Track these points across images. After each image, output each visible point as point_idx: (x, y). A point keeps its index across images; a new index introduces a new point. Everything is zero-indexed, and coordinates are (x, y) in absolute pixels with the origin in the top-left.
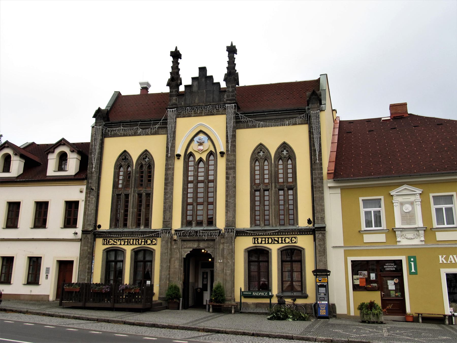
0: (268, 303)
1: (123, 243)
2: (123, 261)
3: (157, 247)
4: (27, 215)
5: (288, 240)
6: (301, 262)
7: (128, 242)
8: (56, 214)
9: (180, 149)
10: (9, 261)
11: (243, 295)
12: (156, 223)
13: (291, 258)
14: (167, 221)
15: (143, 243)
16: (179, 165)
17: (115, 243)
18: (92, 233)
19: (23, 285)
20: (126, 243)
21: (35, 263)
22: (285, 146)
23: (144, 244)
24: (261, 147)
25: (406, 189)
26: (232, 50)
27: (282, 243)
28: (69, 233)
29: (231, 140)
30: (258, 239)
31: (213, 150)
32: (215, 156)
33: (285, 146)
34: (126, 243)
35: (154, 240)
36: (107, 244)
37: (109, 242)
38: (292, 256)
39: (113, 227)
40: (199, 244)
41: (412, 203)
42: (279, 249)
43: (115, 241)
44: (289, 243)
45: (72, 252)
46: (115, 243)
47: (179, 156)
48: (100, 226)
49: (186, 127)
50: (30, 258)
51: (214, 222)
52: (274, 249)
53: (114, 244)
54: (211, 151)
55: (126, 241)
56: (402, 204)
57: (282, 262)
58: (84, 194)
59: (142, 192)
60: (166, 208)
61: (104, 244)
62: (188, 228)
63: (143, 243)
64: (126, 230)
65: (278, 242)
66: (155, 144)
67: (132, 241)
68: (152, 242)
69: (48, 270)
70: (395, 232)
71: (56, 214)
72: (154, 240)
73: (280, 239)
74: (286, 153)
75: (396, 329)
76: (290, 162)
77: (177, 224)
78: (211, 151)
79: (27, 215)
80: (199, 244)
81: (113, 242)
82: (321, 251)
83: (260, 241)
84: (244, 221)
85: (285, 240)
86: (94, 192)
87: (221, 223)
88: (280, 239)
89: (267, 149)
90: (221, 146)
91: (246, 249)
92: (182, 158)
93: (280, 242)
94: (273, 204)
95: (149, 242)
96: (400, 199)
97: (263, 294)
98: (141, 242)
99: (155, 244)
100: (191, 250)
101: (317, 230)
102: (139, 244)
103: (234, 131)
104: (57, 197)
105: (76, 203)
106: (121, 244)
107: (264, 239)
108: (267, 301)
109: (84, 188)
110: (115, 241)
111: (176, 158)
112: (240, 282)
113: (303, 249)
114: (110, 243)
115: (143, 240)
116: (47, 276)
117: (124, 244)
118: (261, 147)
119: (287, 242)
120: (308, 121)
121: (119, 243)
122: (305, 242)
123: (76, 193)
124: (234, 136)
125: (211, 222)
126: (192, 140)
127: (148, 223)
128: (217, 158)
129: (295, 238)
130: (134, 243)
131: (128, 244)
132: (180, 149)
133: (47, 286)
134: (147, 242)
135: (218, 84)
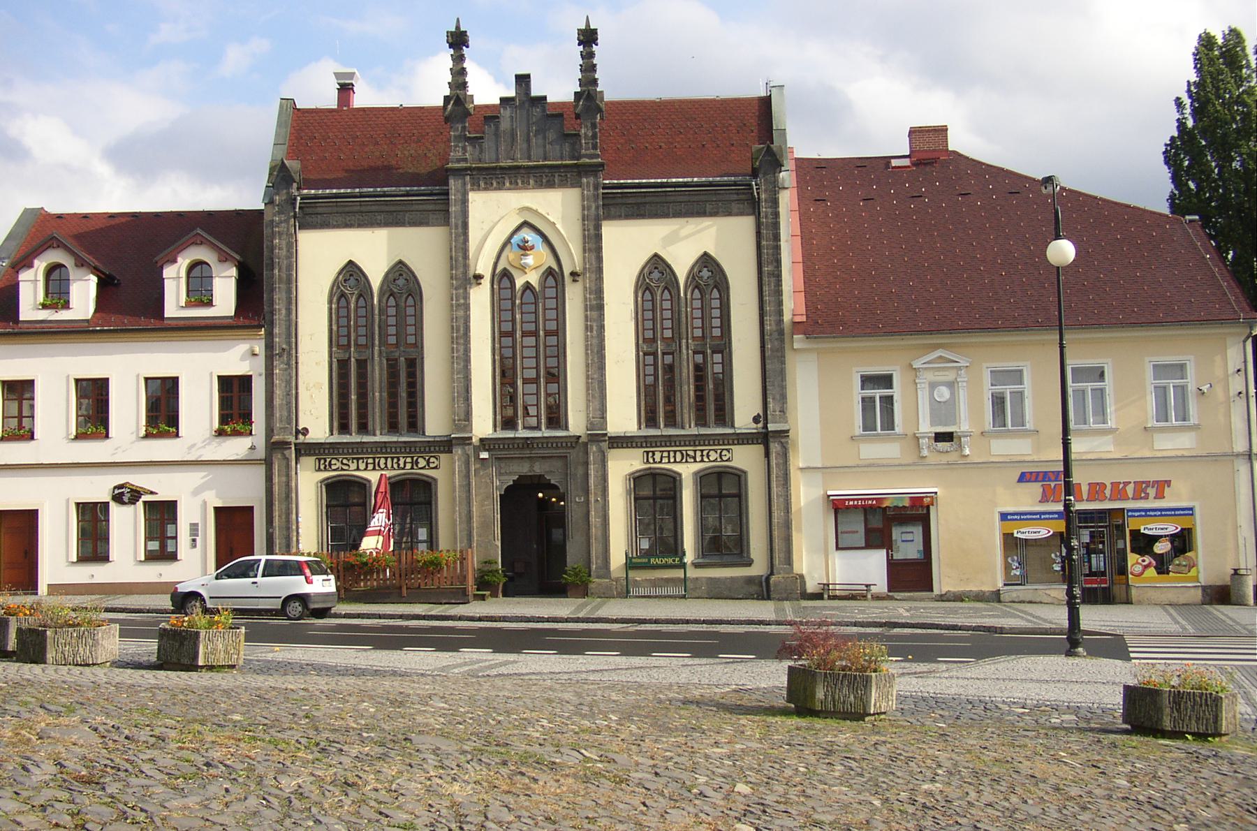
0: (679, 579)
1: (362, 466)
3: (443, 474)
4: (127, 408)
5: (713, 456)
6: (740, 496)
8: (198, 407)
9: (483, 264)
10: (27, 521)
11: (630, 565)
12: (435, 423)
13: (720, 490)
15: (408, 466)
16: (480, 299)
18: (283, 449)
20: (370, 467)
22: (706, 260)
24: (657, 264)
25: (941, 357)
26: (588, 38)
27: (702, 461)
28: (237, 447)
29: (593, 244)
30: (653, 453)
31: (555, 267)
32: (560, 279)
33: (706, 260)
34: (370, 467)
35: (432, 460)
37: (330, 464)
38: (722, 489)
39: (335, 432)
40: (532, 466)
41: (951, 385)
42: (696, 474)
44: (715, 460)
47: (478, 277)
48: (305, 432)
49: (492, 214)
51: (419, 424)
52: (687, 471)
54: (550, 268)
55: (370, 461)
56: (933, 386)
57: (703, 498)
58: (261, 360)
59: (397, 354)
60: (466, 391)
61: (319, 470)
62: (510, 434)
63: (408, 466)
64: (366, 439)
65: (694, 458)
66: (419, 247)
67: (383, 461)
68: (428, 462)
69: (194, 528)
70: (918, 438)
71: (198, 407)
72: (432, 460)
73: (698, 453)
74: (709, 273)
75: (916, 609)
76: (715, 294)
77: (483, 424)
78: (550, 268)
79: (127, 408)
80: (532, 466)
81: (339, 465)
82: (777, 478)
83: (657, 458)
84: (623, 415)
85: (708, 456)
86: (281, 354)
87: (576, 423)
88: (698, 453)
89: (669, 266)
90: (573, 257)
91: (630, 474)
92: (486, 282)
93: (698, 459)
95: (422, 463)
96: (930, 376)
97: (670, 561)
99: (435, 468)
101: (768, 437)
102: (399, 468)
103: (598, 228)
104: (199, 370)
105: (245, 381)
106: (358, 469)
107: (665, 454)
108: (679, 574)
109: (259, 347)
111: (473, 281)
112: (619, 543)
113: (745, 472)
115: (409, 460)
116: (194, 540)
118: (657, 264)
119: (712, 459)
120: (751, 205)
121: (353, 466)
122: (745, 458)
123: (238, 357)
124: (599, 237)
125: (556, 417)
126: (507, 242)
127: (415, 424)
128: (563, 285)
129: (728, 450)
130: (389, 465)
131: (374, 469)
132: (483, 264)
134: (417, 463)
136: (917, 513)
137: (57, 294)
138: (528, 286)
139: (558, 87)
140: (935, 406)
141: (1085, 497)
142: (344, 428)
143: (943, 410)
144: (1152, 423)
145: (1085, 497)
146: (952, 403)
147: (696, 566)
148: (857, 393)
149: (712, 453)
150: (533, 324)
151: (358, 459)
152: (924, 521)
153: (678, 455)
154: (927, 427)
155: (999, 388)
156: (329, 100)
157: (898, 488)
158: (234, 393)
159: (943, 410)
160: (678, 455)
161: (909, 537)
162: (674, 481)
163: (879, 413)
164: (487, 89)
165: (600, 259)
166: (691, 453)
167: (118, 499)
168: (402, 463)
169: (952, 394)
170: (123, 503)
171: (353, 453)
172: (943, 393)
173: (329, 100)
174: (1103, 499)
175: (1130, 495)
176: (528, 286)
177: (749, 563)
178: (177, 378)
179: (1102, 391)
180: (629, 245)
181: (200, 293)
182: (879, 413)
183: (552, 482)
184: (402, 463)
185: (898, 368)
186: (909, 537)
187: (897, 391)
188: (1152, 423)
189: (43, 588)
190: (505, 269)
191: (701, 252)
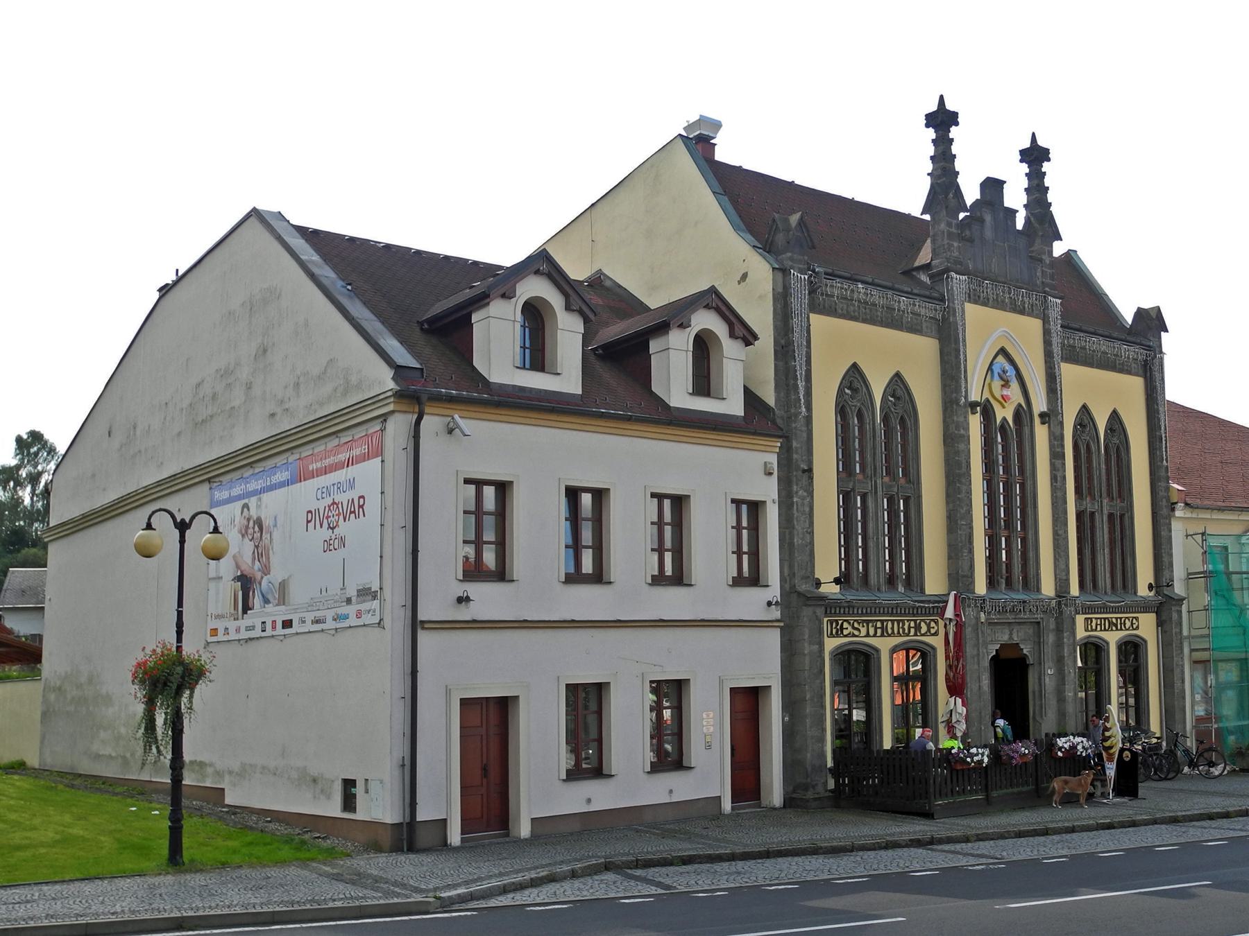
1: (872, 632)
2: (1120, 695)
7: (882, 628)
12: (934, 582)
14: (959, 577)
15: (912, 631)
17: (856, 633)
18: (800, 601)
19: (646, 776)
20: (879, 631)
21: (586, 703)
23: (916, 635)
28: (753, 603)
34: (879, 631)
36: (837, 635)
37: (842, 628)
43: (856, 625)
45: (760, 661)
46: (856, 633)
50: (572, 689)
53: (854, 636)
55: (879, 625)
63: (912, 631)
81: (850, 629)
86: (794, 474)
94: (1104, 495)
95: (924, 629)
98: (909, 628)
100: (998, 647)
106: (868, 635)
110: (856, 625)
114: (845, 632)
117: (875, 635)
131: (882, 635)
133: (709, 775)
135: (1013, 212)
151: (868, 622)
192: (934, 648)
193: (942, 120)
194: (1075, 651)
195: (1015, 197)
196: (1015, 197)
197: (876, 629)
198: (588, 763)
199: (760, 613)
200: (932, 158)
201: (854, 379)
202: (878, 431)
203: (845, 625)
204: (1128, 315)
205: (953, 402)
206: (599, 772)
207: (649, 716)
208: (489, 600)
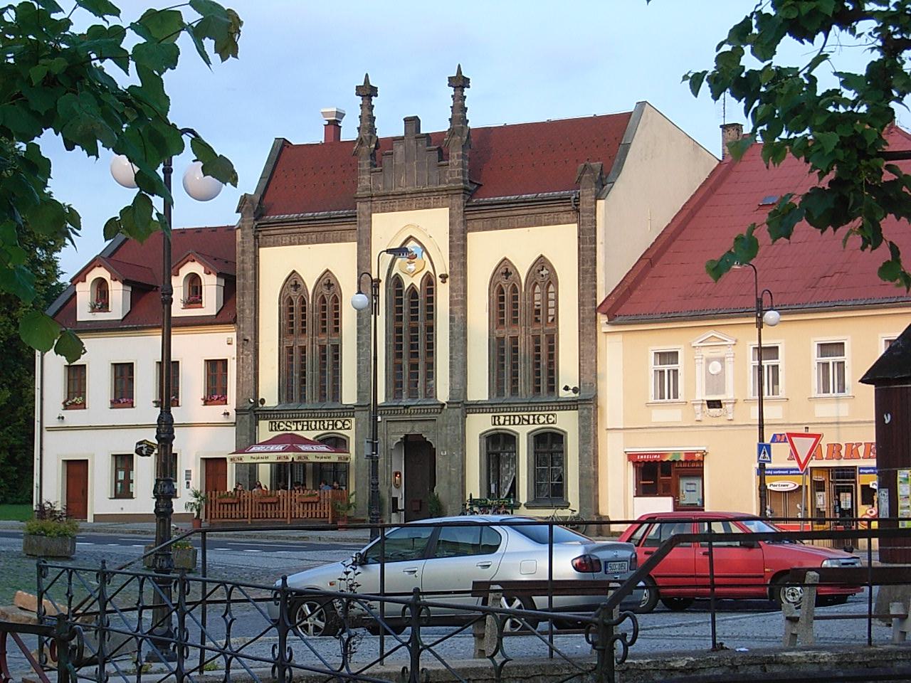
1: (300, 427)
5: (542, 419)
12: (349, 395)
17: (289, 428)
18: (251, 412)
20: (305, 428)
23: (333, 429)
27: (534, 423)
28: (215, 413)
31: (432, 271)
34: (305, 428)
35: (346, 422)
37: (279, 426)
38: (549, 445)
41: (722, 360)
43: (289, 424)
44: (544, 423)
46: (289, 428)
52: (523, 433)
53: (287, 430)
55: (305, 423)
56: (708, 361)
61: (272, 430)
63: (330, 427)
65: (528, 421)
68: (344, 424)
72: (346, 422)
73: (531, 417)
74: (543, 271)
81: (285, 426)
84: (479, 389)
85: (538, 419)
86: (249, 344)
88: (531, 417)
93: (531, 421)
95: (339, 425)
96: (707, 353)
101: (586, 402)
106: (297, 430)
107: (507, 418)
110: (289, 424)
113: (565, 433)
114: (281, 428)
115: (331, 423)
117: (302, 430)
121: (294, 428)
122: (566, 422)
123: (221, 343)
131: (308, 429)
134: (336, 425)
136: (693, 467)
137: (101, 300)
138: (412, 287)
139: (436, 121)
140: (709, 377)
141: (824, 456)
142: (290, 399)
143: (715, 381)
144: (652, 400)
145: (824, 456)
146: (721, 376)
147: (528, 506)
148: (815, 357)
149: (541, 417)
150: (410, 314)
151: (297, 422)
152: (699, 473)
153: (517, 418)
154: (702, 395)
155: (660, 367)
156: (318, 137)
157: (673, 446)
158: (216, 369)
159: (715, 381)
160: (517, 418)
161: (692, 488)
162: (511, 439)
163: (667, 385)
164: (389, 126)
165: (464, 265)
166: (526, 417)
167: (139, 452)
168: (326, 425)
169: (723, 367)
170: (142, 455)
171: (292, 418)
172: (715, 367)
173: (318, 137)
174: (839, 458)
175: (862, 455)
176: (412, 287)
177: (567, 506)
178: (133, 364)
179: (676, 371)
180: (491, 247)
181: (195, 297)
182: (667, 385)
183: (428, 440)
184: (326, 425)
185: (682, 347)
186: (692, 488)
187: (681, 366)
188: (814, 394)
189: (90, 519)
190: (397, 274)
191: (539, 255)
192: (348, 438)
193: (460, 83)
194: (892, 388)
195: (771, 164)
196: (771, 164)
197: (303, 426)
198: (123, 490)
199: (222, 419)
200: (450, 119)
201: (294, 282)
202: (310, 312)
203: (281, 424)
204: (78, 148)
205: (367, 283)
206: (129, 496)
207: (133, 475)
208: (74, 417)
